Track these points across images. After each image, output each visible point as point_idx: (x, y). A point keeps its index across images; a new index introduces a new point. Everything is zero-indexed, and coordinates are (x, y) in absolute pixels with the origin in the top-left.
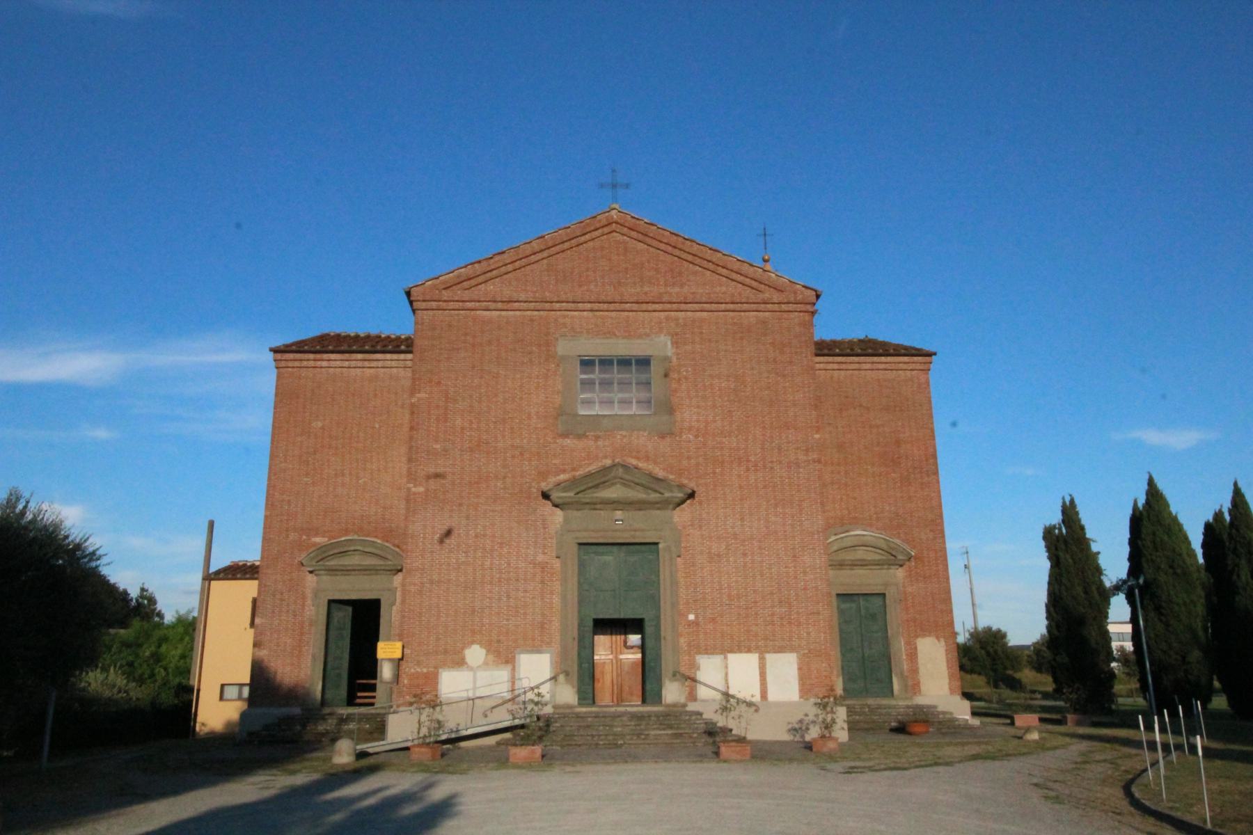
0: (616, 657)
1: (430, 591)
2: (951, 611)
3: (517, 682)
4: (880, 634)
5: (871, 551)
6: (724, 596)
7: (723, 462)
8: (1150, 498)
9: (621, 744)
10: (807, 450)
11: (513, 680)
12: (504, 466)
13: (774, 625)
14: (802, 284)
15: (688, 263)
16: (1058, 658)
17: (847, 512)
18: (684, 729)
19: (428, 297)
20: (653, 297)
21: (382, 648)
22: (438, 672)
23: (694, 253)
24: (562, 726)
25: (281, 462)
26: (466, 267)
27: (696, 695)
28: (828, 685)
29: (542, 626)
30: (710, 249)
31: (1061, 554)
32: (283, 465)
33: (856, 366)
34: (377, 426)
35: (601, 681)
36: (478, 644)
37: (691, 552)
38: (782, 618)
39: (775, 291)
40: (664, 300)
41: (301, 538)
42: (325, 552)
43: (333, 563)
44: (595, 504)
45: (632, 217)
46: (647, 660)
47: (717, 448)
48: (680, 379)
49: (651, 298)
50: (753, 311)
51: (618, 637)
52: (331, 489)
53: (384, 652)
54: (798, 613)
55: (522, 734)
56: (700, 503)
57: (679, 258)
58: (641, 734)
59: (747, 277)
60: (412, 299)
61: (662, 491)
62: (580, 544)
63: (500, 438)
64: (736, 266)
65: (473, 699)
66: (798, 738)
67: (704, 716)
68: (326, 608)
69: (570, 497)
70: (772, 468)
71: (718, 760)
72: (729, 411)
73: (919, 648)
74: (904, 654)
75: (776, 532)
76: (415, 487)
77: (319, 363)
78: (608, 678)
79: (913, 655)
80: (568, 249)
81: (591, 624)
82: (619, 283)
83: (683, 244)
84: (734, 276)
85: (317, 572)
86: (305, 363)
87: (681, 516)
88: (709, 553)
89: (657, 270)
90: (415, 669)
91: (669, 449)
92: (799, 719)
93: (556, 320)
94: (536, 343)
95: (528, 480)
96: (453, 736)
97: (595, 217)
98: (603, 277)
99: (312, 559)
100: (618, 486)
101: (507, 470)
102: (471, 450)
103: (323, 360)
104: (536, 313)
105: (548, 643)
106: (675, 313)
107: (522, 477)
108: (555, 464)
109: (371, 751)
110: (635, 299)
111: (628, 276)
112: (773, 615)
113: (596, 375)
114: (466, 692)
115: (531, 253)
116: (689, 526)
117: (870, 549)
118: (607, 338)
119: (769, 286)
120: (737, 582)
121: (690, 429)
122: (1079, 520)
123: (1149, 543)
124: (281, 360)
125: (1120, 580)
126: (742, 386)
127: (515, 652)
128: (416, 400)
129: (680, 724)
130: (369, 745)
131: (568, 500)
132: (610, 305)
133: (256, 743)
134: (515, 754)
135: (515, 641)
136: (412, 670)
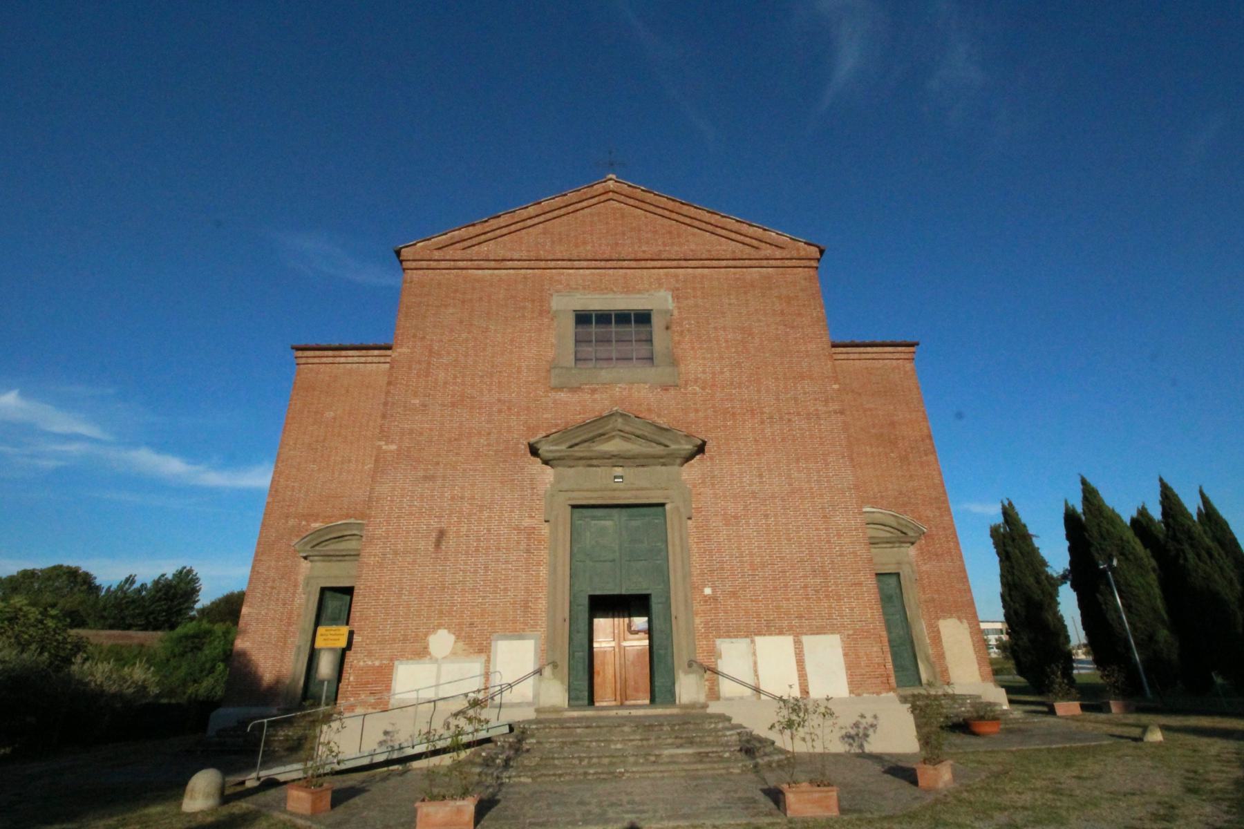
0: (619, 645)
1: (394, 563)
2: (969, 591)
3: (492, 677)
5: (881, 530)
7: (734, 414)
9: (620, 773)
10: (826, 401)
15: (686, 226)
16: (1020, 643)
18: (708, 744)
21: (322, 635)
22: (393, 666)
25: (290, 450)
29: (526, 606)
31: (1009, 549)
32: (292, 452)
35: (601, 672)
36: (445, 628)
37: (703, 513)
40: (663, 257)
41: (300, 524)
42: (321, 536)
44: (591, 459)
46: (655, 648)
47: (727, 400)
48: (682, 331)
51: (621, 620)
52: (336, 475)
53: (325, 640)
56: (712, 458)
57: (677, 221)
58: (649, 755)
60: (401, 258)
62: (574, 507)
63: (486, 392)
65: (434, 701)
66: (855, 750)
67: (733, 722)
68: (317, 595)
74: (927, 638)
75: (801, 489)
76: (386, 444)
77: (338, 360)
78: (610, 671)
79: (937, 639)
80: (564, 215)
82: (617, 244)
83: (680, 208)
84: (733, 236)
85: (311, 558)
86: (324, 360)
87: (691, 472)
88: (725, 514)
90: (364, 662)
95: (515, 436)
96: (395, 755)
99: (306, 544)
101: (492, 426)
102: (453, 405)
105: (532, 626)
108: (547, 419)
109: (282, 778)
110: (632, 256)
111: (626, 238)
112: (806, 587)
113: (594, 329)
115: (527, 217)
118: (603, 294)
120: (760, 547)
122: (1020, 520)
124: (302, 357)
126: (750, 338)
129: (704, 736)
131: (558, 454)
132: (608, 263)
135: (492, 623)
136: (361, 663)
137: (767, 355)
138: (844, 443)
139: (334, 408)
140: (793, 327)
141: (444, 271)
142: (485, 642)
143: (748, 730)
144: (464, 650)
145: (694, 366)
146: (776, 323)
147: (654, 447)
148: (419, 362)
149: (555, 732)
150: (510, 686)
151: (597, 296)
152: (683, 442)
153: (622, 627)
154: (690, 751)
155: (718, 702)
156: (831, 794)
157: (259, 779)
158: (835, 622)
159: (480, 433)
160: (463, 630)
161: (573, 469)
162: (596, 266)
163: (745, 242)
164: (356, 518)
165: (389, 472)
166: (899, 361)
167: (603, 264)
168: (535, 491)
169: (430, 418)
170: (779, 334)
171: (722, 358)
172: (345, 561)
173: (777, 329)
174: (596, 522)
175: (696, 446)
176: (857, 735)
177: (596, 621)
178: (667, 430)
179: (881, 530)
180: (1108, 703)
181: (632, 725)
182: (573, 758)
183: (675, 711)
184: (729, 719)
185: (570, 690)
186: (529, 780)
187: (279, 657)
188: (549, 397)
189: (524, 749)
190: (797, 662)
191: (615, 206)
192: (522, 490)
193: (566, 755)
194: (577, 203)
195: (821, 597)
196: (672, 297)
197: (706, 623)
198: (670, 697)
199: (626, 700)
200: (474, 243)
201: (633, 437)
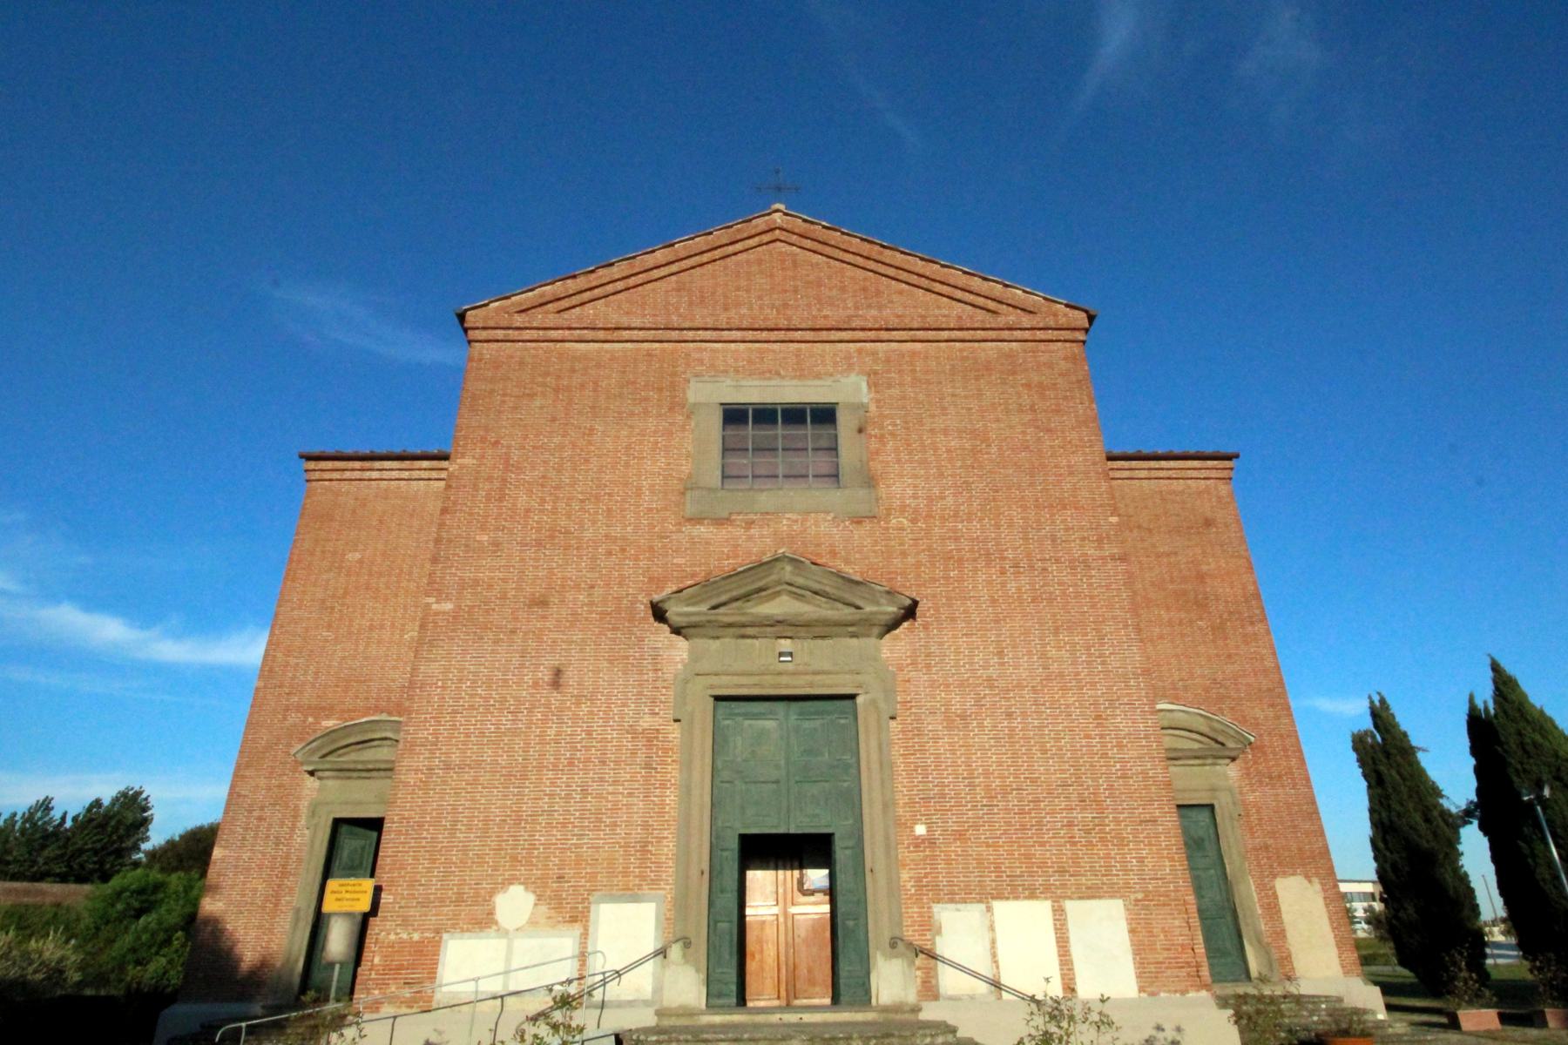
0: (785, 913)
1: (445, 783)
3: (591, 960)
4: (1212, 872)
7: (960, 560)
10: (1100, 540)
19: (491, 324)
22: (440, 941)
25: (293, 610)
27: (937, 985)
31: (1382, 768)
33: (1126, 474)
35: (757, 957)
36: (520, 884)
37: (913, 710)
38: (1088, 832)
40: (854, 325)
41: (304, 721)
42: (334, 741)
43: (352, 757)
44: (744, 626)
47: (950, 538)
51: (789, 873)
52: (361, 648)
54: (1117, 821)
56: (926, 627)
60: (466, 325)
61: (859, 602)
62: (718, 699)
67: (959, 1034)
68: (328, 831)
69: (698, 614)
74: (1258, 908)
75: (1061, 675)
77: (367, 474)
78: (770, 951)
79: (1272, 908)
80: (708, 263)
81: (734, 844)
82: (786, 305)
83: (881, 253)
84: (959, 294)
85: (320, 774)
86: (348, 475)
87: (895, 646)
89: (843, 289)
90: (397, 934)
92: (1146, 1037)
93: (688, 355)
94: (656, 386)
98: (760, 298)
99: (313, 752)
100: (785, 598)
101: (597, 575)
104: (657, 345)
107: (620, 584)
108: (679, 565)
110: (810, 324)
112: (1070, 825)
116: (908, 665)
119: (1015, 307)
121: (903, 509)
124: (315, 470)
126: (984, 446)
128: (457, 467)
131: (694, 619)
132: (771, 333)
136: (392, 937)
144: (550, 918)
145: (900, 487)
148: (490, 479)
150: (618, 974)
151: (756, 383)
152: (883, 601)
153: (789, 885)
155: (934, 1004)
159: (577, 587)
164: (390, 714)
166: (1208, 482)
167: (764, 335)
172: (369, 778)
178: (857, 583)
180: (1543, 1013)
183: (870, 1016)
184: (953, 1030)
194: (727, 245)
199: (796, 998)
201: (810, 593)
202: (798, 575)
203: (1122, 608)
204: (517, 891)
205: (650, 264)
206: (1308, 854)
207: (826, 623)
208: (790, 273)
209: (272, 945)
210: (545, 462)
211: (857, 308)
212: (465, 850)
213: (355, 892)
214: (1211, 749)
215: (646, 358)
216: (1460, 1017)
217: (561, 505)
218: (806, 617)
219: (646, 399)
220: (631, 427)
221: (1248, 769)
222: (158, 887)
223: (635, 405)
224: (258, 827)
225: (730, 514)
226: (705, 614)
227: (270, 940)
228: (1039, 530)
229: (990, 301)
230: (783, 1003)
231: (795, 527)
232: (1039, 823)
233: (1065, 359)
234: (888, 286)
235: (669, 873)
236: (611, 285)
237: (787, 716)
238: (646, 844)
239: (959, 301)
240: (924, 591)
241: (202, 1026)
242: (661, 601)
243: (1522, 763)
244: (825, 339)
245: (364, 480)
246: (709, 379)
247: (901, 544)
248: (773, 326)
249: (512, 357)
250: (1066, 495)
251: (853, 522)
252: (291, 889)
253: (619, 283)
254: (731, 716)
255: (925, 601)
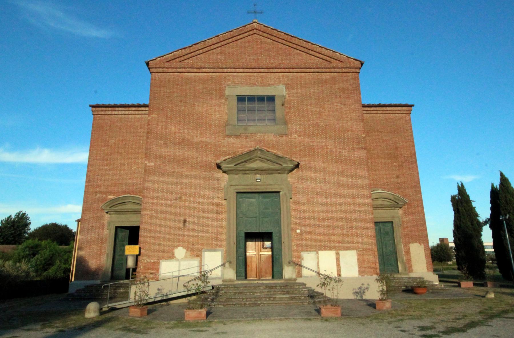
2: (426, 230)
5: (386, 201)
6: (316, 220)
7: (314, 149)
8: (502, 181)
9: (259, 304)
10: (359, 143)
11: (201, 266)
12: (197, 152)
13: (343, 235)
14: (353, 58)
16: (460, 254)
17: (372, 182)
18: (296, 294)
19: (158, 66)
20: (275, 65)
22: (159, 262)
23: (297, 43)
24: (225, 293)
25: (94, 160)
26: (178, 51)
28: (374, 268)
29: (217, 237)
30: (305, 41)
31: (460, 208)
33: (375, 112)
34: (141, 142)
35: (250, 266)
36: (181, 246)
37: (297, 196)
39: (339, 62)
40: (281, 67)
41: (103, 196)
42: (113, 203)
44: (245, 171)
45: (265, 26)
47: (311, 142)
48: (290, 107)
49: (274, 66)
50: (328, 72)
51: (259, 243)
53: (129, 251)
54: (356, 228)
55: (202, 297)
56: (302, 171)
58: (271, 297)
59: (324, 55)
60: (149, 67)
61: (281, 163)
62: (238, 193)
64: (319, 50)
65: (178, 277)
67: (307, 286)
68: (114, 230)
69: (231, 167)
70: (340, 152)
71: (319, 317)
72: (317, 123)
73: (411, 248)
74: (403, 252)
76: (149, 163)
77: (114, 112)
78: (254, 265)
79: (408, 253)
80: (231, 42)
81: (243, 235)
82: (258, 59)
83: (291, 39)
84: (318, 55)
85: (110, 213)
86: (107, 112)
87: (292, 177)
89: (278, 53)
90: (147, 260)
91: (285, 142)
92: (359, 287)
93: (225, 77)
96: (165, 298)
97: (245, 26)
98: (249, 56)
99: (107, 206)
100: (258, 161)
103: (115, 111)
104: (214, 74)
106: (287, 73)
107: (206, 157)
108: (224, 151)
109: (118, 307)
110: (266, 66)
112: (343, 230)
113: (246, 105)
114: (172, 273)
115: (212, 44)
116: (296, 182)
117: (385, 199)
118: (251, 86)
119: (336, 60)
120: (323, 212)
122: (466, 193)
123: (504, 202)
124: (95, 111)
125: (487, 219)
126: (323, 110)
127: (202, 250)
128: (151, 118)
130: (118, 303)
131: (230, 169)
133: (70, 300)
134: (189, 314)
135: (202, 245)
137: (331, 119)
138: (365, 163)
139: (114, 138)
140: (345, 105)
141: (171, 74)
142: (199, 252)
143: (312, 289)
144: (190, 256)
145: (295, 125)
146: (337, 103)
147: (275, 165)
148: (162, 122)
149: (232, 289)
150: (211, 270)
151: (248, 88)
152: (289, 163)
153: (259, 246)
154: (288, 296)
155: (301, 278)
156: (338, 309)
157: (108, 307)
158: (355, 245)
159: (193, 158)
160: (189, 247)
161: (237, 175)
162: (247, 72)
163: (323, 58)
164: (130, 194)
165: (151, 176)
166: (403, 115)
167: (251, 70)
168: (220, 185)
169: (168, 150)
170: (338, 108)
171: (309, 121)
172: (126, 214)
173: (337, 106)
174: (249, 200)
175: (295, 165)
176: (360, 292)
177: (248, 243)
178: (281, 157)
179: (386, 201)
180: (487, 283)
181: (264, 286)
182: (240, 298)
183: (282, 281)
184: (305, 285)
185: (237, 273)
186: (222, 306)
187: (99, 258)
188: (225, 140)
189: (219, 295)
190: (337, 262)
191: (257, 37)
192: (214, 185)
193: (237, 297)
194: (237, 36)
195: (349, 234)
196: (286, 88)
197: (297, 245)
198: (280, 276)
199: (261, 277)
200: (185, 58)
201: (266, 160)
202: (262, 154)
203: (364, 164)
204: (180, 248)
205: (210, 44)
206: (421, 236)
207: (269, 169)
208: (259, 46)
209: (101, 264)
210: (179, 116)
211: (282, 60)
212: (164, 237)
213: (134, 249)
214: (395, 205)
215: (211, 79)
216: (461, 284)
217: (186, 131)
218: (265, 168)
219: (212, 94)
220: (207, 104)
221: (405, 211)
222: (37, 246)
223: (208, 96)
224: (92, 229)
225: (241, 134)
226: (233, 167)
227: (100, 262)
228: (339, 139)
229: (328, 57)
230: (258, 278)
231: (261, 138)
232: (334, 229)
233: (352, 79)
234: (293, 51)
235: (225, 244)
236: (198, 51)
237: (259, 198)
238: (217, 235)
239: (317, 57)
240: (302, 159)
241: (85, 287)
242: (220, 163)
243: (505, 207)
244: (272, 72)
245: (113, 114)
246: (232, 86)
247: (295, 144)
248: (254, 67)
249: (165, 78)
250: (349, 127)
251: (280, 136)
252: (105, 247)
253: (200, 50)
254: (242, 198)
255: (302, 162)
